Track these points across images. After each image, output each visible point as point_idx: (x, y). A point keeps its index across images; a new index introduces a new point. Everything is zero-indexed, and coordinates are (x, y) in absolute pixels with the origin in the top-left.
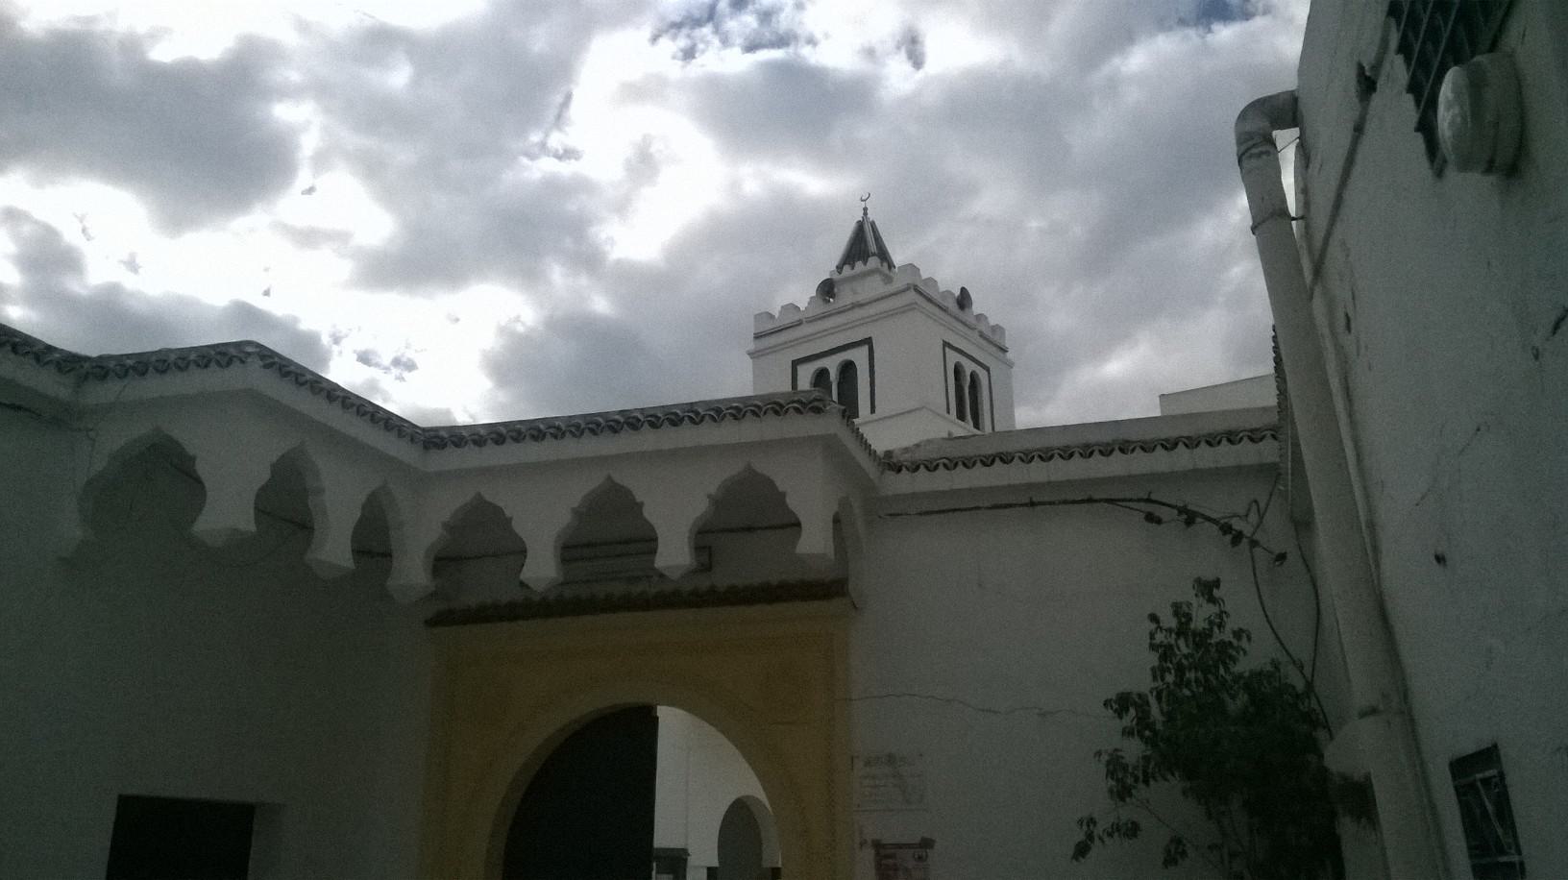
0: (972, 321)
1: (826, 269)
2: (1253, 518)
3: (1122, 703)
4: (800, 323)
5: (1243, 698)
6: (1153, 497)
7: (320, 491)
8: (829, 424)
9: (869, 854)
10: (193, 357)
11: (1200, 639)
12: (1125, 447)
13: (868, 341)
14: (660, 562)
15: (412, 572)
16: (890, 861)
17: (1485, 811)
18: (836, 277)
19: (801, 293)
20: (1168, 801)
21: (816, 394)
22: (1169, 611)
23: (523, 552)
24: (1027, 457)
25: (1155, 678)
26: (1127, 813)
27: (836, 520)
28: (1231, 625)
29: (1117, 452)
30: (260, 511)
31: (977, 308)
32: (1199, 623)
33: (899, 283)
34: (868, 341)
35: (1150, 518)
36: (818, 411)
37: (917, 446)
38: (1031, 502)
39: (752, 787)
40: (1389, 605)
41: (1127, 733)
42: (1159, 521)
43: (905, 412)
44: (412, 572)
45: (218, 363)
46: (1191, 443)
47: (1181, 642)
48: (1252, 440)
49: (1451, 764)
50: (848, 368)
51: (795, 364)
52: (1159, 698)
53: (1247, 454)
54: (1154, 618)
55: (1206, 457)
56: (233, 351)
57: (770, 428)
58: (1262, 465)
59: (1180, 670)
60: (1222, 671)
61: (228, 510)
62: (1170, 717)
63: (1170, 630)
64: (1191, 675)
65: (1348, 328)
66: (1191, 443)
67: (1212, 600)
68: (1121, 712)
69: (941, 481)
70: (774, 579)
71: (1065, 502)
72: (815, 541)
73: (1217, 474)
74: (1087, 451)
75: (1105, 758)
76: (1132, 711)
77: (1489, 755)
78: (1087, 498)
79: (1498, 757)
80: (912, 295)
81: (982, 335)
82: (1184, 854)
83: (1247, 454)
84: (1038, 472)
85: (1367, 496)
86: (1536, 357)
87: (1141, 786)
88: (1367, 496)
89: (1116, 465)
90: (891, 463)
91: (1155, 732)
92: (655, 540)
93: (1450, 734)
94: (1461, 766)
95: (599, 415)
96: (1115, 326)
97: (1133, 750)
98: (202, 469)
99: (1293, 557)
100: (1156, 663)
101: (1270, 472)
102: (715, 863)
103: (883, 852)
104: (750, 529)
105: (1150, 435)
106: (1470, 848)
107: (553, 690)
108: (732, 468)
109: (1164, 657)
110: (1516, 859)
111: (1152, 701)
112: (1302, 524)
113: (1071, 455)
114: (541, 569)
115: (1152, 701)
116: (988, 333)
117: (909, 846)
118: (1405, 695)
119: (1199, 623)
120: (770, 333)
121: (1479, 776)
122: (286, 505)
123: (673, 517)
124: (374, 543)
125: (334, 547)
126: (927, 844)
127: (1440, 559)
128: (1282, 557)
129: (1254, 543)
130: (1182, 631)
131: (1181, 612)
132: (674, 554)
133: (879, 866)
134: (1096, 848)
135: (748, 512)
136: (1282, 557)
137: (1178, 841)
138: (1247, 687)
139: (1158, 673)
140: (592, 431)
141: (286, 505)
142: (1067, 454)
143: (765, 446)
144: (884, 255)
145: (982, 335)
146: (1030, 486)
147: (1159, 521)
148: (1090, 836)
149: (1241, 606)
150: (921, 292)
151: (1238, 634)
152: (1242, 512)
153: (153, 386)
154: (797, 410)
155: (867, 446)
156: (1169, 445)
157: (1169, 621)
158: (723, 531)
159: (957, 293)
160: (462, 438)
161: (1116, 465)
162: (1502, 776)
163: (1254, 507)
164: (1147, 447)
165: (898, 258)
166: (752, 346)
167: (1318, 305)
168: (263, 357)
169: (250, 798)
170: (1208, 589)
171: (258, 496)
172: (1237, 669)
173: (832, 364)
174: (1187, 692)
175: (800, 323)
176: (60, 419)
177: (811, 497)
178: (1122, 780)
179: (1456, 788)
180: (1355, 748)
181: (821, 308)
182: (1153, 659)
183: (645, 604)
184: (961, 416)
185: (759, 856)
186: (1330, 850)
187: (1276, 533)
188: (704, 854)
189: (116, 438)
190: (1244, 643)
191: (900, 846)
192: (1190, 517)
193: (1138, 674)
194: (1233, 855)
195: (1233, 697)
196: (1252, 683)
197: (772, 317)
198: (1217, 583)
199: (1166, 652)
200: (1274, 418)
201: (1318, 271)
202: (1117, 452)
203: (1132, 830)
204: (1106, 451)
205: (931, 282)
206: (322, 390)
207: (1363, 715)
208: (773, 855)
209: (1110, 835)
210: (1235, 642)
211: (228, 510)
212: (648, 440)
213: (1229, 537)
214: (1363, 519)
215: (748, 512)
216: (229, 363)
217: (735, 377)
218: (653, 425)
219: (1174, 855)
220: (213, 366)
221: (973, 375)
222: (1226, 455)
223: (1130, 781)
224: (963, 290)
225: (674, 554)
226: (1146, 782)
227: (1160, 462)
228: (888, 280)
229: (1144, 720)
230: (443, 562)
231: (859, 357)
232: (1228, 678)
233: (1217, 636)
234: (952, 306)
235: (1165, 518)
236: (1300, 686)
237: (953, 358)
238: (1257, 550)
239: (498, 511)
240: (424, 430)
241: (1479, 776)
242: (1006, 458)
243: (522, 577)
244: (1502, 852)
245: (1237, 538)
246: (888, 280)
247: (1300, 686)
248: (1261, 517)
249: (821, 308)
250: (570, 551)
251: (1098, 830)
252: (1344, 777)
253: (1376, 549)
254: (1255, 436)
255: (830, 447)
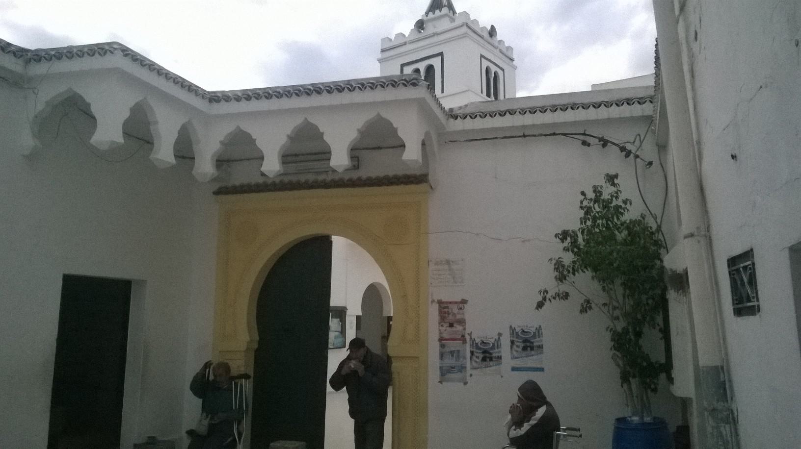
0: (496, 44)
1: (420, 14)
2: (637, 143)
3: (564, 235)
4: (405, 44)
5: (625, 233)
6: (587, 133)
7: (156, 123)
8: (420, 92)
9: (436, 306)
10: (86, 50)
11: (606, 205)
12: (574, 107)
13: (441, 54)
14: (333, 163)
15: (205, 167)
16: (446, 310)
17: (742, 280)
18: (425, 18)
19: (407, 27)
20: (585, 283)
21: (414, 76)
22: (592, 190)
23: (262, 158)
24: (523, 112)
25: (581, 223)
26: (564, 288)
27: (423, 144)
28: (622, 196)
29: (569, 109)
30: (126, 134)
31: (499, 37)
32: (606, 196)
33: (458, 22)
34: (441, 54)
35: (584, 143)
36: (414, 85)
37: (466, 106)
38: (524, 135)
39: (380, 278)
40: (704, 183)
41: (566, 249)
42: (589, 145)
43: (460, 88)
44: (205, 167)
45: (100, 54)
46: (608, 105)
47: (596, 205)
48: (639, 103)
49: (728, 261)
50: (430, 69)
51: (402, 66)
52: (583, 233)
53: (637, 110)
54: (583, 193)
55: (615, 112)
56: (107, 47)
57: (390, 94)
58: (643, 116)
59: (595, 219)
60: (615, 220)
61: (109, 131)
62: (587, 242)
63: (591, 200)
64: (600, 222)
65: (696, 38)
66: (608, 105)
67: (613, 184)
68: (563, 240)
69: (478, 124)
70: (391, 174)
71: (541, 135)
72: (412, 154)
73: (621, 121)
74: (554, 109)
75: (554, 262)
76: (569, 239)
77: (748, 255)
78: (552, 133)
79: (753, 255)
80: (464, 29)
81: (501, 51)
82: (590, 308)
83: (637, 110)
84: (528, 120)
85: (698, 128)
86: (797, 45)
87: (571, 275)
88: (698, 128)
89: (570, 116)
90: (452, 115)
91: (579, 248)
92: (330, 153)
93: (728, 245)
94: (733, 262)
95: (301, 86)
96: (574, 44)
97: (568, 258)
98: (94, 109)
99: (656, 163)
100: (583, 215)
101: (648, 120)
102: (360, 314)
103: (443, 306)
104: (380, 148)
105: (586, 101)
106: (733, 300)
107: (279, 227)
108: (298, 121)
109: (586, 213)
110: (755, 303)
111: (579, 235)
112: (662, 147)
113: (545, 111)
114: (272, 166)
115: (579, 235)
116: (504, 50)
117: (456, 303)
118: (708, 229)
119: (606, 196)
120: (389, 49)
121: (742, 265)
122: (139, 131)
123: (340, 141)
124: (185, 152)
125: (164, 152)
126: (464, 302)
127: (734, 157)
128: (650, 163)
129: (637, 157)
130: (596, 201)
131: (597, 191)
132: (340, 160)
133: (440, 312)
134: (547, 303)
135: (378, 138)
136: (650, 163)
137: (588, 301)
138: (628, 228)
139: (583, 220)
140: (297, 94)
141: (139, 131)
142: (543, 110)
143: (384, 103)
144: (451, 7)
145: (501, 51)
146: (524, 127)
147: (589, 145)
148: (544, 299)
149: (627, 188)
150: (469, 27)
151: (625, 202)
152: (632, 140)
153: (65, 66)
154: (404, 84)
155: (440, 105)
156: (597, 106)
157: (591, 195)
158: (364, 149)
159: (489, 28)
160: (228, 97)
161: (570, 116)
162: (753, 264)
163: (638, 138)
164: (585, 107)
165: (458, 9)
166: (380, 56)
167: (681, 24)
168: (123, 51)
169: (126, 276)
170: (611, 179)
171: (124, 124)
172: (623, 219)
173: (422, 67)
174: (597, 230)
175: (405, 44)
176: (17, 83)
177: (410, 130)
178: (562, 272)
179: (730, 272)
180: (680, 257)
181: (417, 36)
182: (582, 213)
183: (326, 185)
184: (488, 95)
185: (382, 311)
186: (663, 305)
187: (648, 151)
188: (354, 309)
189: (47, 93)
190: (628, 206)
191: (450, 303)
192: (605, 143)
193: (573, 223)
194: (615, 308)
195: (620, 233)
196: (630, 227)
197: (390, 40)
198: (616, 176)
199: (588, 211)
200: (651, 92)
201: (682, 8)
202: (569, 109)
203: (566, 296)
204: (564, 109)
205: (475, 22)
206: (154, 69)
207: (685, 237)
208: (390, 309)
209: (554, 298)
210: (623, 206)
211: (109, 131)
212: (325, 100)
213: (624, 153)
214: (695, 140)
215: (378, 138)
216: (105, 53)
217: (372, 70)
218: (329, 92)
219: (586, 307)
220: (97, 55)
221: (496, 73)
222: (626, 111)
223: (565, 273)
224: (492, 27)
225: (340, 160)
226: (574, 274)
227: (592, 114)
228: (453, 20)
229: (574, 243)
230: (221, 162)
231: (436, 62)
232: (619, 223)
233: (614, 203)
234: (486, 35)
235: (592, 143)
236: (654, 228)
237: (486, 64)
238: (638, 160)
239: (248, 136)
240: (209, 92)
241: (742, 265)
242: (512, 112)
243: (263, 169)
244: (749, 301)
245: (628, 154)
246: (453, 20)
247: (654, 228)
248: (641, 142)
249: (417, 36)
250: (287, 158)
251: (548, 296)
252: (671, 270)
253: (700, 154)
254: (641, 101)
255: (421, 104)
